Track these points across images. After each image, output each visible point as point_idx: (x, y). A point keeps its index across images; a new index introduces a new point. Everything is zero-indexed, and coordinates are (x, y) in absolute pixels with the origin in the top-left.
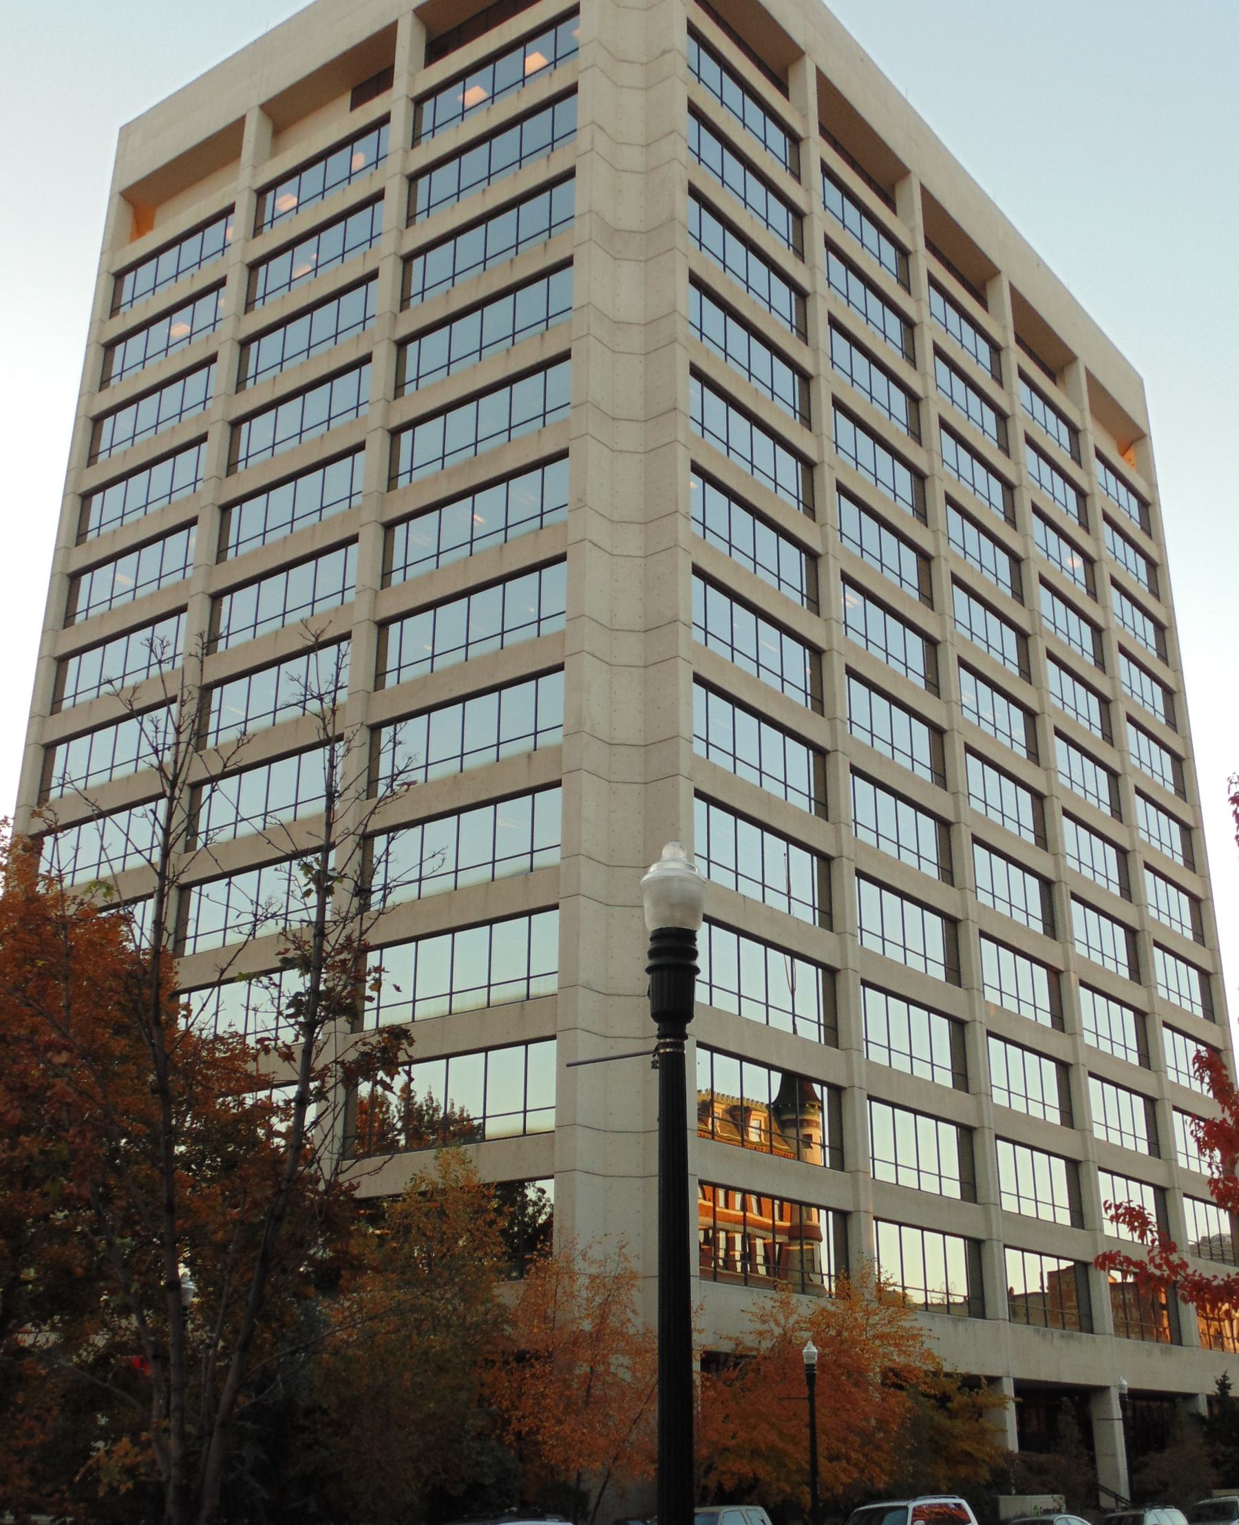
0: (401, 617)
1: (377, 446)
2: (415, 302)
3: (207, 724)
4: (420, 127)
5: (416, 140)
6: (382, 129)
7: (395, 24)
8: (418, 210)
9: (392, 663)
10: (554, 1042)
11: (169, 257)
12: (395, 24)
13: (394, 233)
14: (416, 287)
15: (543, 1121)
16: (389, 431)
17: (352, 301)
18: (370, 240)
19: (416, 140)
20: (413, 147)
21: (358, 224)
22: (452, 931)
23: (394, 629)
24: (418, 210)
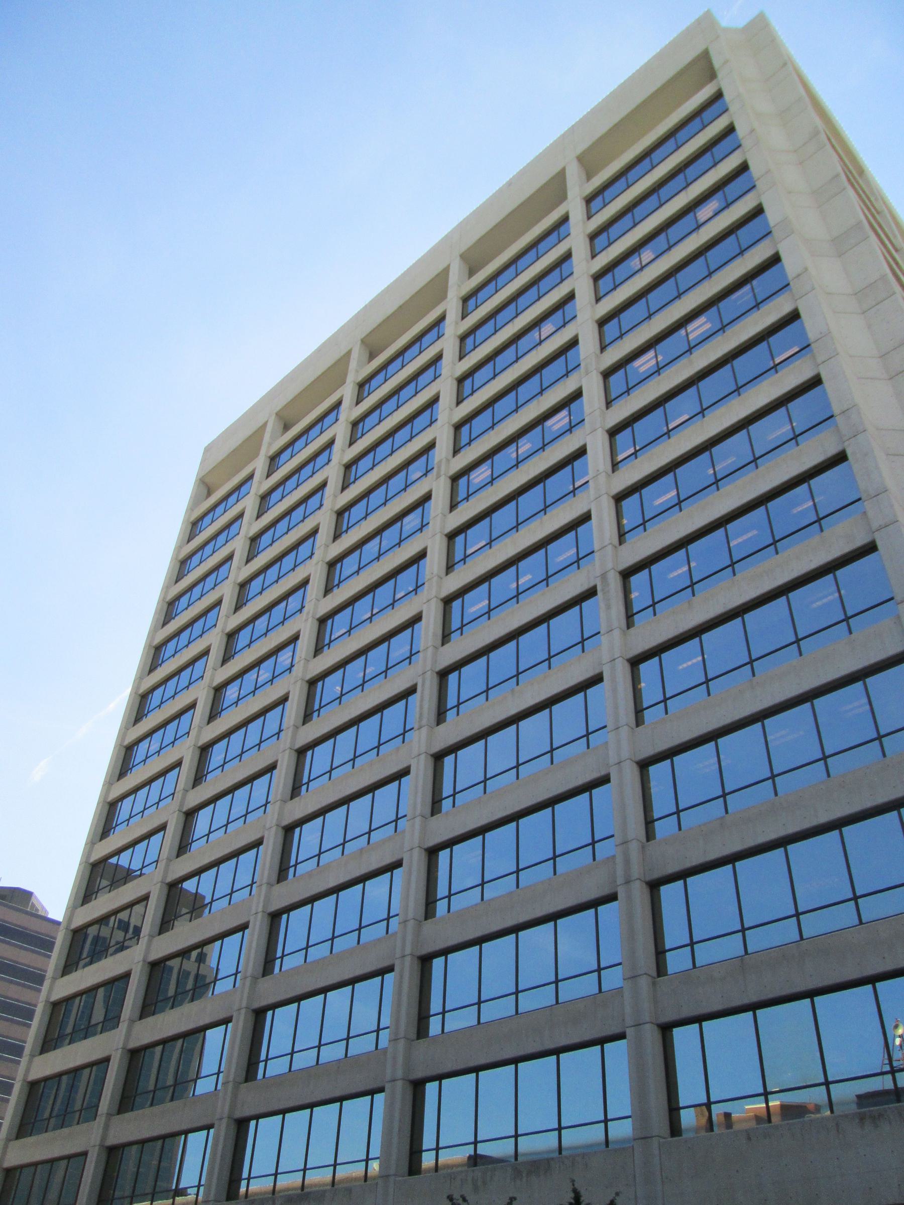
0: (450, 844)
1: (416, 863)
2: (451, 715)
3: (302, 779)
4: (454, 556)
5: (446, 637)
6: (410, 698)
7: (448, 266)
8: (448, 707)
9: (435, 1006)
10: (623, 1043)
11: (251, 676)
12: (448, 266)
13: (430, 651)
14: (451, 701)
15: (622, 1130)
16: (432, 755)
17: (395, 713)
18: (403, 734)
19: (446, 637)
20: (447, 574)
21: (400, 646)
22: (515, 1061)
23: (444, 855)
24: (448, 707)
